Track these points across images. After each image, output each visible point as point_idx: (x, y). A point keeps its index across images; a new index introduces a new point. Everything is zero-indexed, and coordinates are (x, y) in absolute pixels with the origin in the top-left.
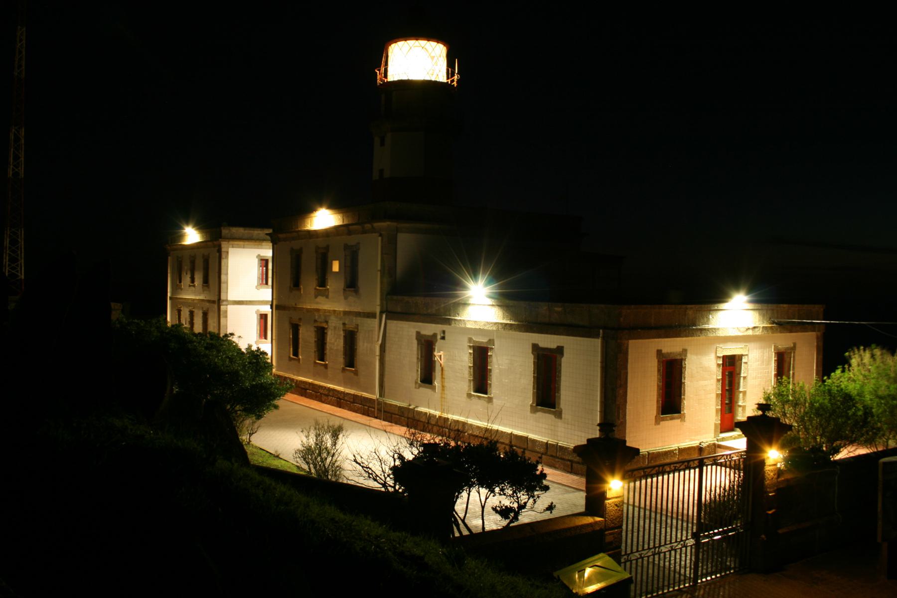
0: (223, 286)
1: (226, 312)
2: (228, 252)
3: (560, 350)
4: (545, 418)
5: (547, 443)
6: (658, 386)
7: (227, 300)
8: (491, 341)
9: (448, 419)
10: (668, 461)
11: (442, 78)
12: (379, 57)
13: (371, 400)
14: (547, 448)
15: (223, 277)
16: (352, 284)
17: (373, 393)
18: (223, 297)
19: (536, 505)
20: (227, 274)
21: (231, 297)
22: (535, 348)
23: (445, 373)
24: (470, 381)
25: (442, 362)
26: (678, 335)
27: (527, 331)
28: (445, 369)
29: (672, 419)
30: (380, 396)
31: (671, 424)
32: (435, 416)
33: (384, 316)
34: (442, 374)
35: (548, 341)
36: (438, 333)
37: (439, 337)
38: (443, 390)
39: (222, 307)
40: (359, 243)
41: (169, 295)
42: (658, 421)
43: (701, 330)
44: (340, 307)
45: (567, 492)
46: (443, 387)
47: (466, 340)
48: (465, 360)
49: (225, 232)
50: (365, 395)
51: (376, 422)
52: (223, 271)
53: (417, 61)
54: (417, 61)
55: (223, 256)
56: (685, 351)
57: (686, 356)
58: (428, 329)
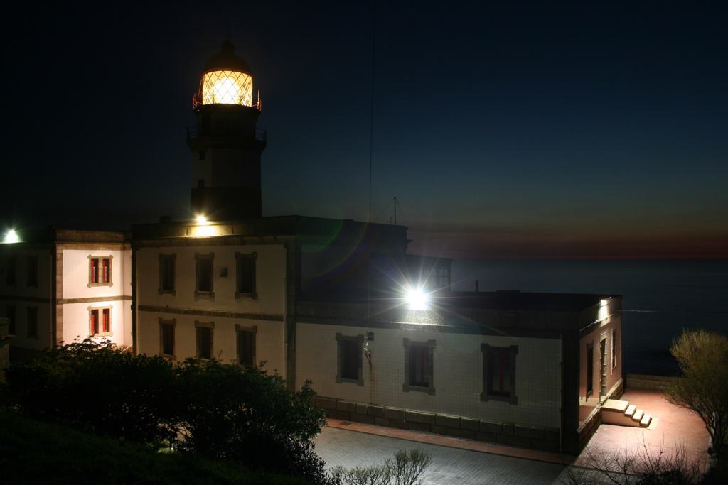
0: (58, 286)
7: (62, 299)
11: (248, 102)
15: (58, 277)
16: (247, 287)
18: (58, 296)
19: (600, 473)
20: (61, 275)
21: (65, 296)
22: (160, 321)
27: (466, 333)
34: (371, 370)
36: (365, 334)
39: (58, 306)
40: (411, 241)
44: (233, 306)
49: (59, 235)
52: (58, 272)
53: (227, 88)
54: (227, 88)
58: (351, 331)
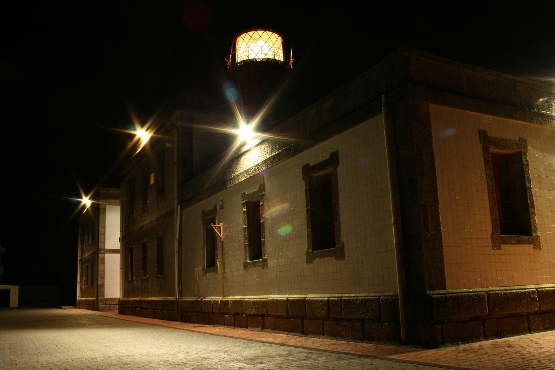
1: (104, 259)
2: (105, 209)
3: (334, 159)
4: (326, 265)
5: (328, 301)
6: (489, 185)
7: (104, 249)
8: (262, 188)
9: (228, 301)
10: (523, 310)
12: (232, 48)
13: (172, 302)
14: (329, 308)
17: (174, 295)
18: (101, 247)
20: (104, 227)
23: (225, 246)
24: (245, 246)
25: (221, 236)
26: (508, 115)
28: (225, 242)
29: (519, 242)
30: (181, 295)
31: (516, 252)
32: (216, 302)
33: (179, 207)
35: (317, 153)
37: (219, 207)
38: (224, 269)
41: (79, 259)
42: (496, 244)
43: (543, 116)
45: (342, 359)
46: (224, 264)
47: (240, 197)
48: (239, 220)
50: (170, 298)
51: (156, 321)
55: (101, 212)
56: (523, 142)
57: (526, 148)
